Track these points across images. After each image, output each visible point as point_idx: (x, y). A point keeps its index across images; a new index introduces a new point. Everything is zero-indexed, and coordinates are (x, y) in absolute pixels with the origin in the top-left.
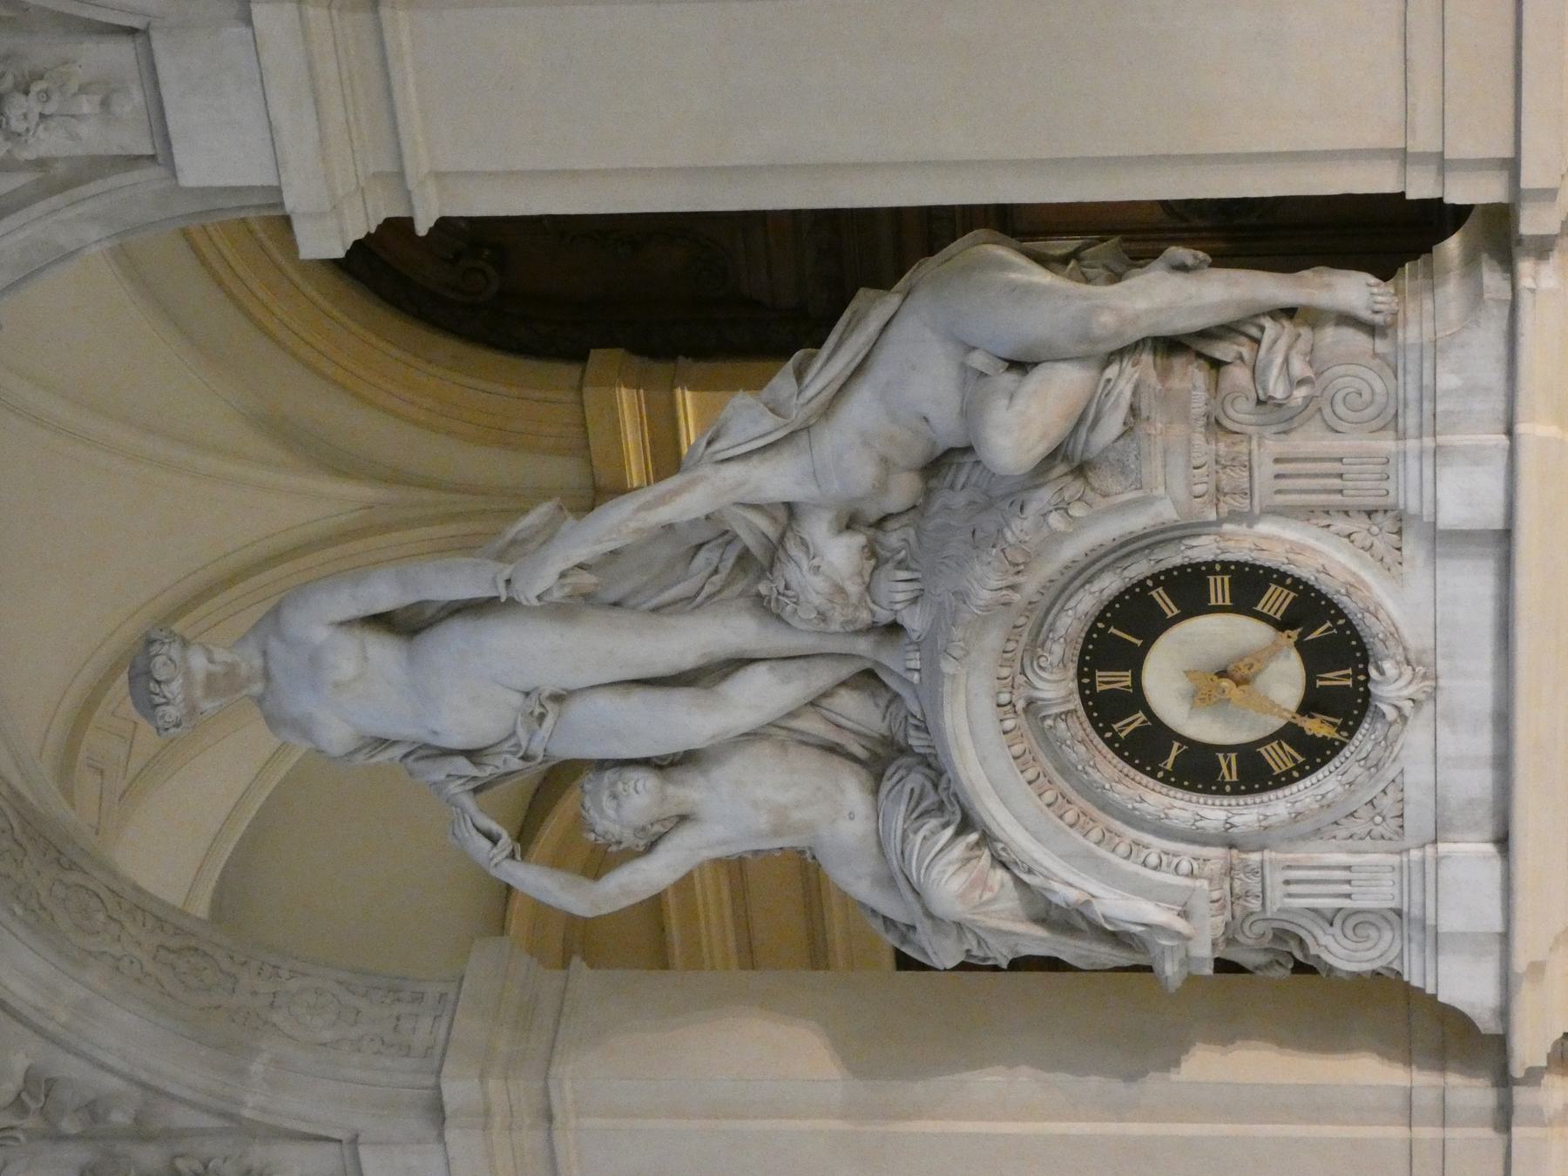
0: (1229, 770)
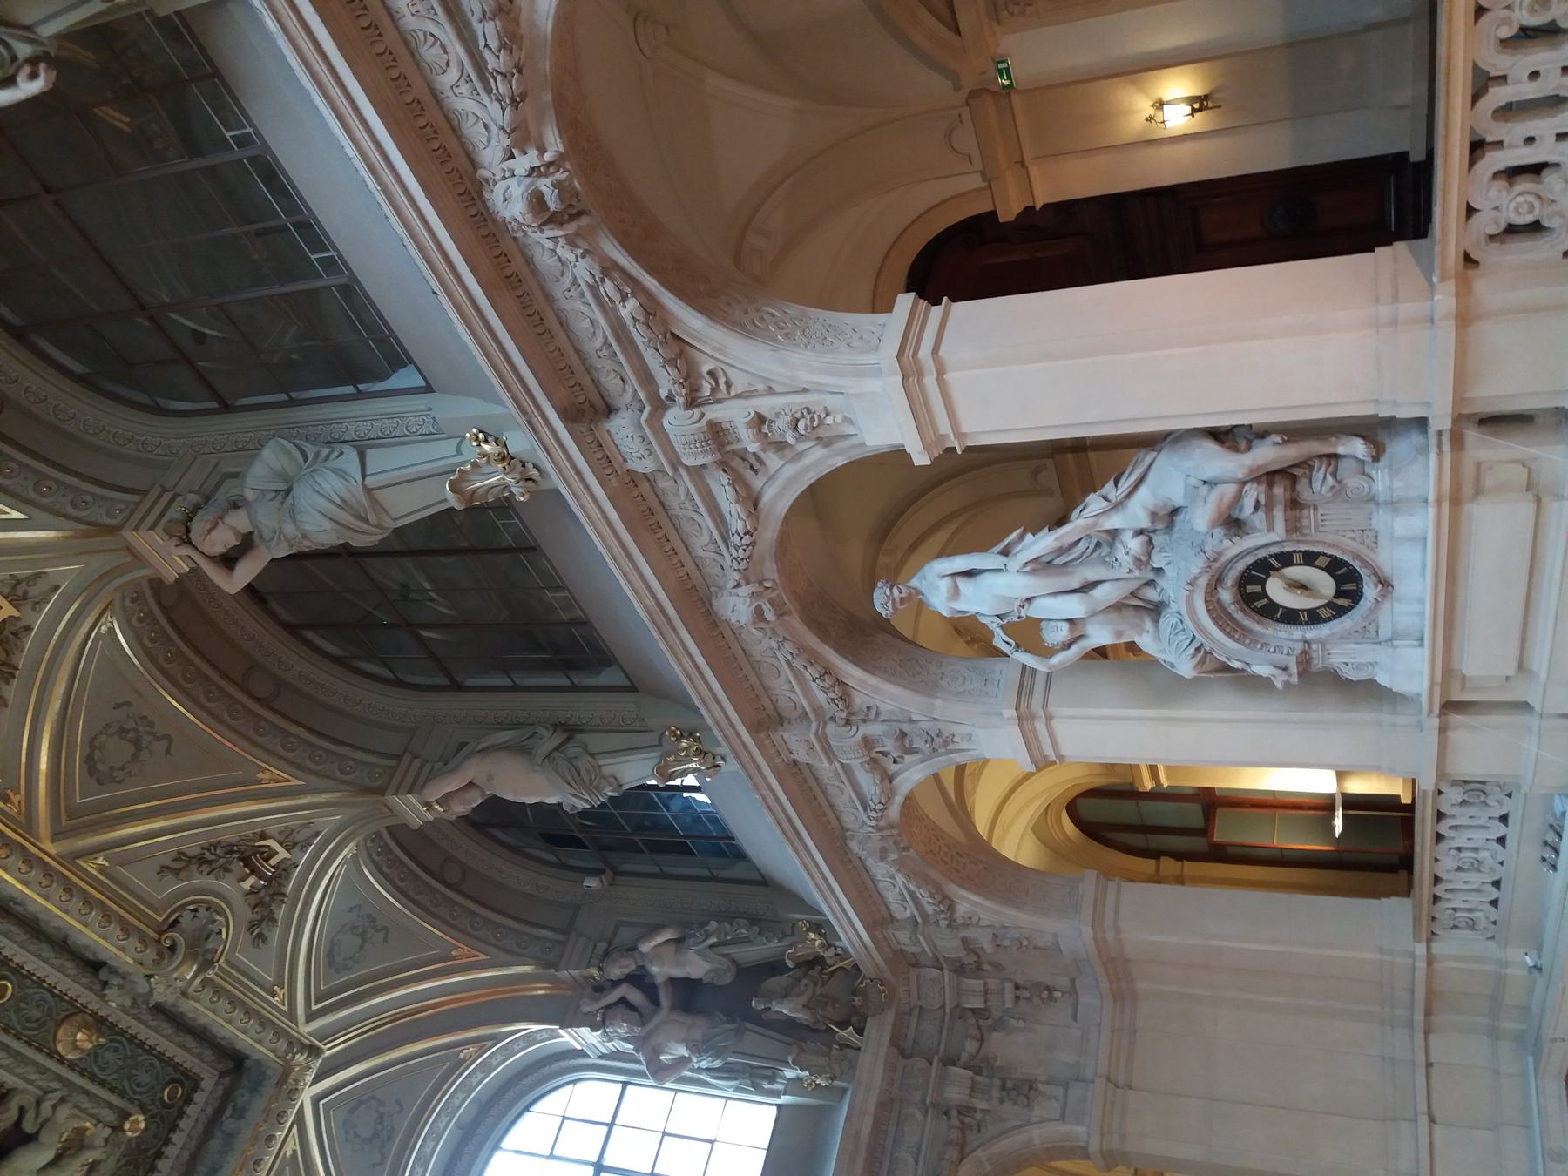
0: (1304, 617)
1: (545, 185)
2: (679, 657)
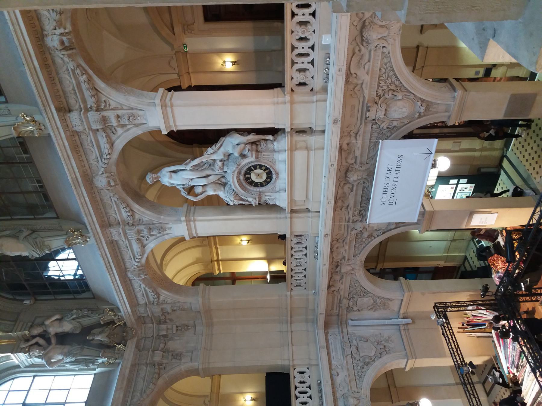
1: (65, 38)
2: (79, 200)
